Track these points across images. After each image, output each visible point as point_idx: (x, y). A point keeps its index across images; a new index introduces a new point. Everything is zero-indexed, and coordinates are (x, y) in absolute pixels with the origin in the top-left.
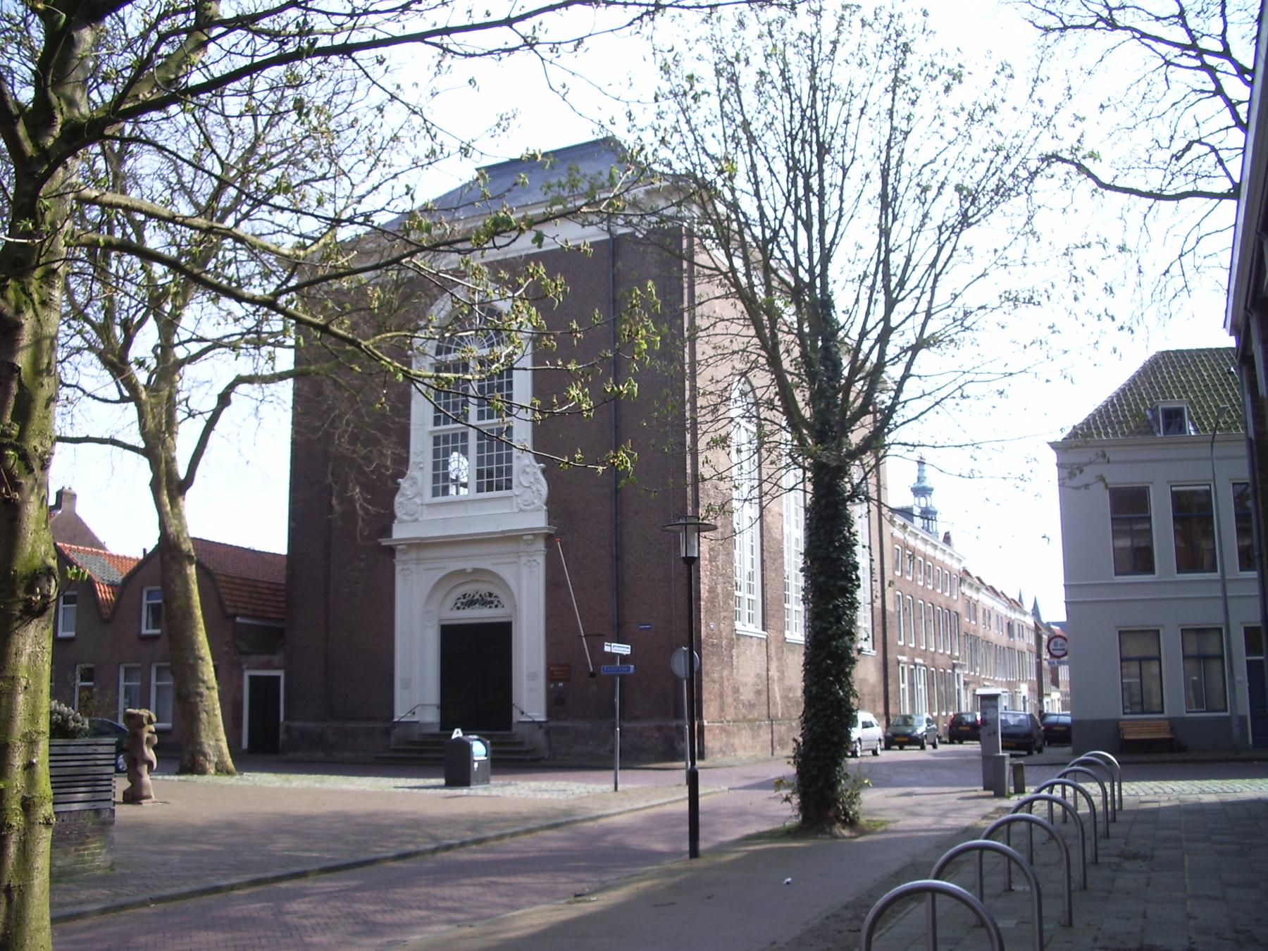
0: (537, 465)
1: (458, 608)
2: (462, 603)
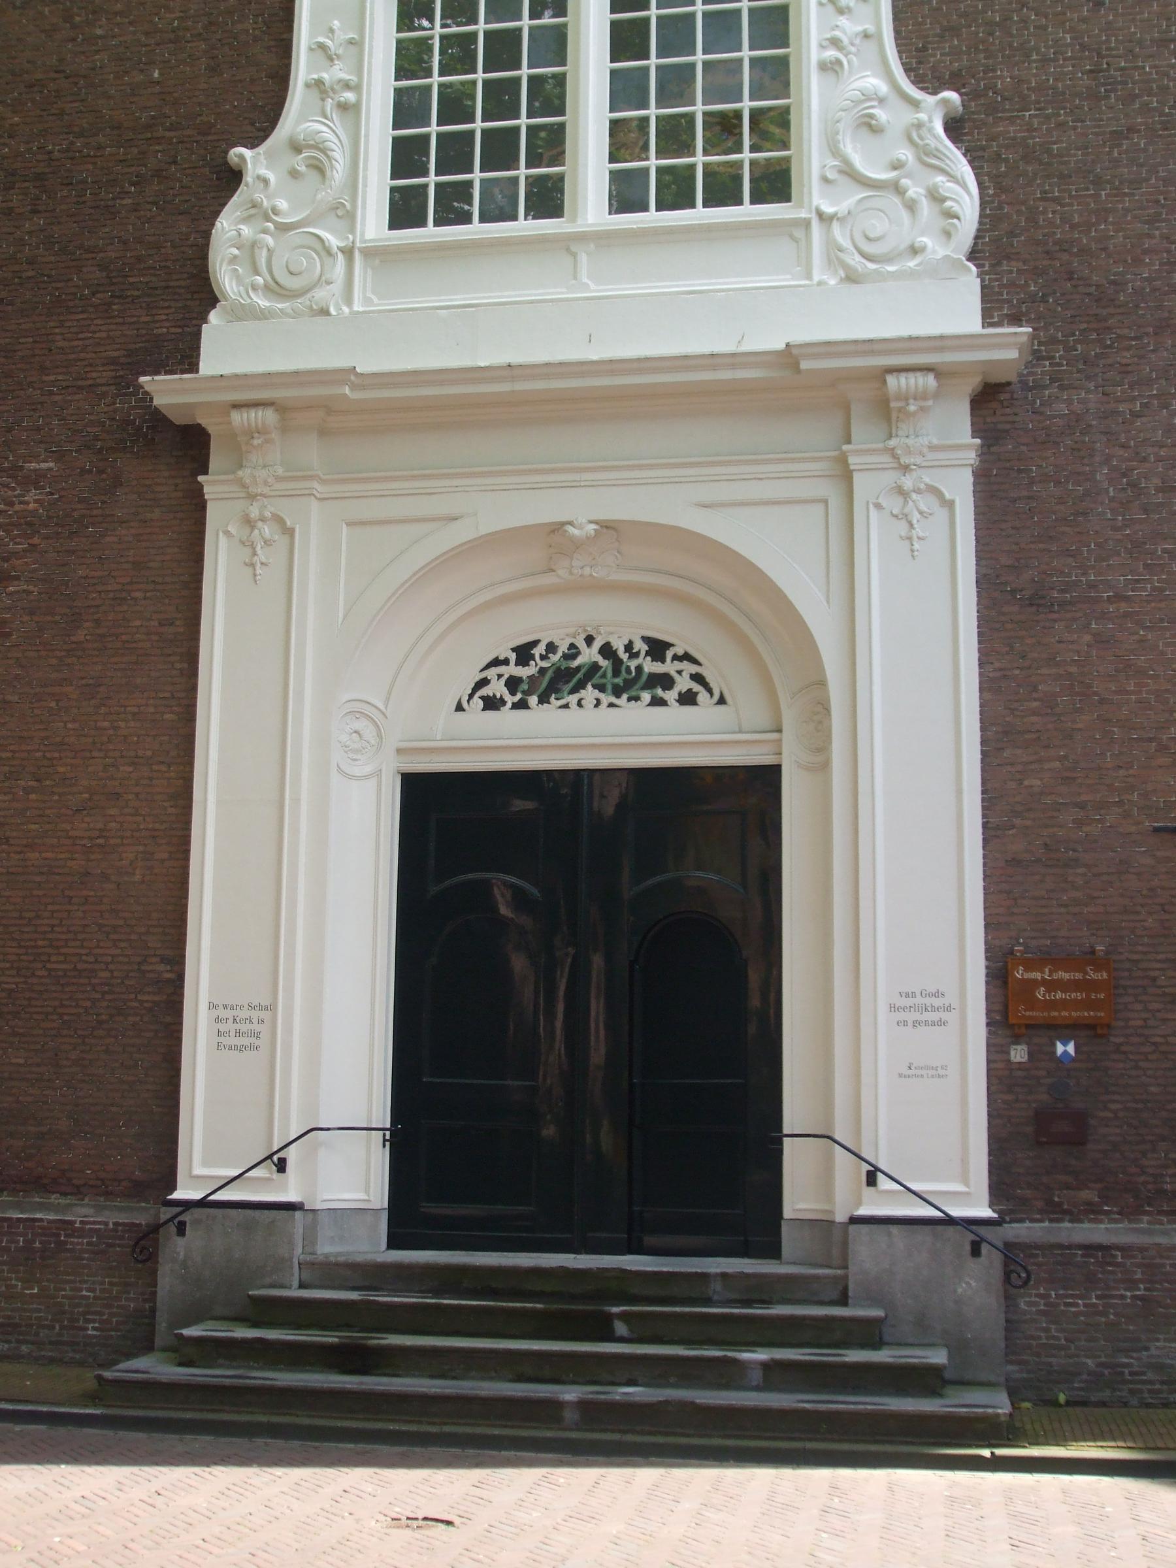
0: (930, 100)
1: (492, 704)
2: (513, 684)
